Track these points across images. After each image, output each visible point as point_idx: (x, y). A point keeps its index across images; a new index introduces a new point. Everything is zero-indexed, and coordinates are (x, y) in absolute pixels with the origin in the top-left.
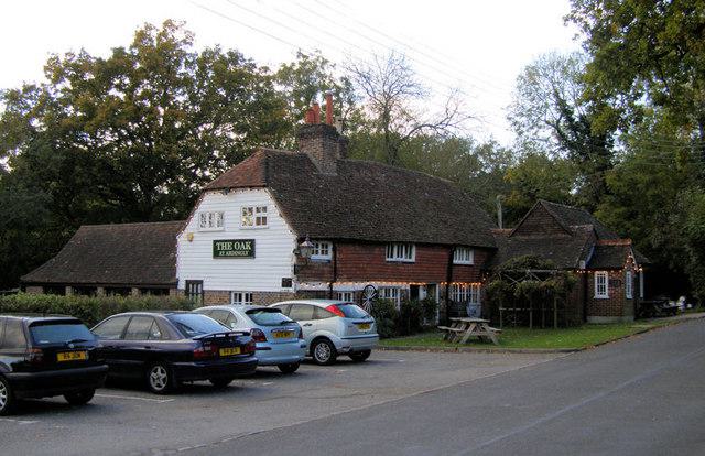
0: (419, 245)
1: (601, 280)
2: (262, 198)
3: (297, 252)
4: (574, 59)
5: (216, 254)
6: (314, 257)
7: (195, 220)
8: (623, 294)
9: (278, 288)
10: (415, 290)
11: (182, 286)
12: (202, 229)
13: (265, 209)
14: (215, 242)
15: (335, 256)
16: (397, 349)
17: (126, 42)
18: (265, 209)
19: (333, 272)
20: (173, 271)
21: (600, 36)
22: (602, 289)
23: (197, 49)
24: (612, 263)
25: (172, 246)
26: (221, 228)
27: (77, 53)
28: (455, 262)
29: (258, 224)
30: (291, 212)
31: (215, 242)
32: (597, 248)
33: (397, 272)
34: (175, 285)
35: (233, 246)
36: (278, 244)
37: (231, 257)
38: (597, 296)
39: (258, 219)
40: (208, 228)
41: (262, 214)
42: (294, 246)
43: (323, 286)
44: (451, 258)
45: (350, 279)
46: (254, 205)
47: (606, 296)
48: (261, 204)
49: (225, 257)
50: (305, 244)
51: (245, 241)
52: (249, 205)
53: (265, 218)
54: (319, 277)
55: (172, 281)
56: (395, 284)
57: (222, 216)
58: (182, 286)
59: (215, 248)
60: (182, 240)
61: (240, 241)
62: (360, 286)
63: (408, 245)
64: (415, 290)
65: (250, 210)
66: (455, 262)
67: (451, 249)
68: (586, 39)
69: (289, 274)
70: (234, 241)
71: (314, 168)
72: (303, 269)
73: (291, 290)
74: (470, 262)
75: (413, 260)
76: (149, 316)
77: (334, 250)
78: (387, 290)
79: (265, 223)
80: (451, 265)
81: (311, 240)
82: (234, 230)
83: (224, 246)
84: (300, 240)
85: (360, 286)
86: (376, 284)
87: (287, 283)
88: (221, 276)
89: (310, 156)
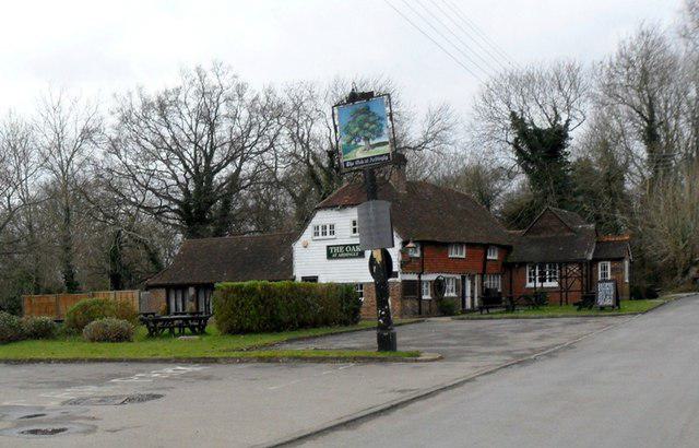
1: (605, 268)
4: (96, 137)
5: (330, 256)
8: (623, 278)
12: (317, 238)
15: (422, 254)
23: (587, 66)
24: (614, 255)
28: (488, 257)
32: (597, 242)
37: (342, 258)
40: (321, 237)
44: (486, 255)
49: (338, 258)
50: (410, 245)
57: (332, 227)
59: (328, 251)
61: (351, 245)
63: (460, 244)
66: (488, 257)
67: (486, 247)
75: (464, 256)
77: (422, 249)
80: (486, 260)
81: (414, 242)
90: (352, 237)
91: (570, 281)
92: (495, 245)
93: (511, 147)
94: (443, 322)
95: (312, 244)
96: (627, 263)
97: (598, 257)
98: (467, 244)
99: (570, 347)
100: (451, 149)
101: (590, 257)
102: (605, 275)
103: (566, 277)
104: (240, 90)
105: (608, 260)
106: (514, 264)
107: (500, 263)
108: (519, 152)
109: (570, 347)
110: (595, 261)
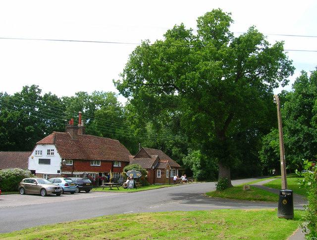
1: (159, 172)
2: (53, 147)
3: (62, 163)
6: (67, 164)
7: (34, 152)
9: (57, 173)
10: (100, 174)
17: (20, 90)
19: (73, 169)
22: (159, 175)
25: (27, 160)
27: (4, 93)
30: (60, 152)
33: (95, 169)
36: (56, 161)
38: (158, 177)
41: (53, 152)
42: (61, 161)
43: (70, 173)
45: (79, 171)
46: (51, 149)
47: (160, 177)
48: (52, 149)
50: (64, 161)
54: (69, 170)
56: (94, 173)
57: (41, 151)
60: (30, 158)
62: (82, 173)
63: (98, 161)
64: (100, 174)
68: (231, 29)
69: (59, 169)
72: (64, 168)
73: (60, 174)
76: (192, 207)
78: (91, 174)
82: (45, 156)
84: (63, 160)
85: (82, 173)
86: (87, 173)
87: (59, 172)
88: (41, 169)
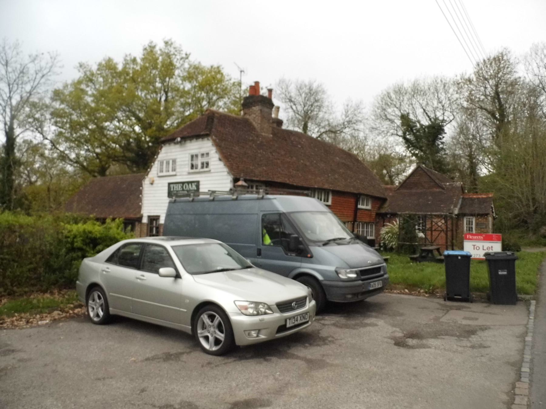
0: (336, 193)
1: (470, 223)
11: (145, 220)
13: (208, 154)
14: (169, 184)
16: (490, 313)
18: (208, 154)
20: (140, 208)
21: (410, 119)
26: (174, 173)
28: (360, 206)
29: (202, 167)
31: (169, 184)
34: (140, 219)
35: (182, 187)
39: (203, 164)
41: (205, 160)
48: (204, 151)
50: (241, 183)
51: (191, 182)
52: (194, 152)
53: (207, 164)
55: (138, 216)
57: (174, 161)
58: (145, 220)
60: (146, 183)
61: (188, 183)
65: (197, 156)
66: (360, 206)
67: (357, 197)
70: (183, 183)
71: (254, 129)
74: (369, 207)
79: (207, 167)
80: (356, 209)
81: (245, 181)
83: (178, 188)
84: (236, 180)
89: (251, 120)
90: (189, 173)
91: (435, 234)
92: (368, 196)
93: (401, 139)
94: (339, 300)
95: (157, 181)
96: (490, 219)
97: (467, 211)
98: (336, 193)
99: (531, 282)
100: (450, 167)
101: (456, 212)
102: (470, 229)
103: (431, 229)
104: (187, 56)
105: (472, 215)
106: (386, 214)
107: (374, 214)
108: (407, 141)
109: (531, 282)
110: (461, 216)
